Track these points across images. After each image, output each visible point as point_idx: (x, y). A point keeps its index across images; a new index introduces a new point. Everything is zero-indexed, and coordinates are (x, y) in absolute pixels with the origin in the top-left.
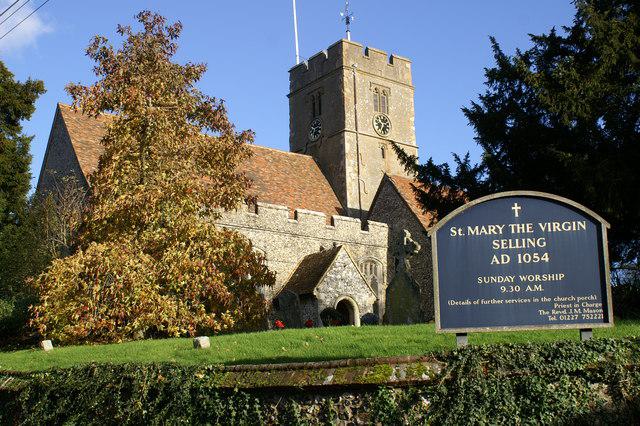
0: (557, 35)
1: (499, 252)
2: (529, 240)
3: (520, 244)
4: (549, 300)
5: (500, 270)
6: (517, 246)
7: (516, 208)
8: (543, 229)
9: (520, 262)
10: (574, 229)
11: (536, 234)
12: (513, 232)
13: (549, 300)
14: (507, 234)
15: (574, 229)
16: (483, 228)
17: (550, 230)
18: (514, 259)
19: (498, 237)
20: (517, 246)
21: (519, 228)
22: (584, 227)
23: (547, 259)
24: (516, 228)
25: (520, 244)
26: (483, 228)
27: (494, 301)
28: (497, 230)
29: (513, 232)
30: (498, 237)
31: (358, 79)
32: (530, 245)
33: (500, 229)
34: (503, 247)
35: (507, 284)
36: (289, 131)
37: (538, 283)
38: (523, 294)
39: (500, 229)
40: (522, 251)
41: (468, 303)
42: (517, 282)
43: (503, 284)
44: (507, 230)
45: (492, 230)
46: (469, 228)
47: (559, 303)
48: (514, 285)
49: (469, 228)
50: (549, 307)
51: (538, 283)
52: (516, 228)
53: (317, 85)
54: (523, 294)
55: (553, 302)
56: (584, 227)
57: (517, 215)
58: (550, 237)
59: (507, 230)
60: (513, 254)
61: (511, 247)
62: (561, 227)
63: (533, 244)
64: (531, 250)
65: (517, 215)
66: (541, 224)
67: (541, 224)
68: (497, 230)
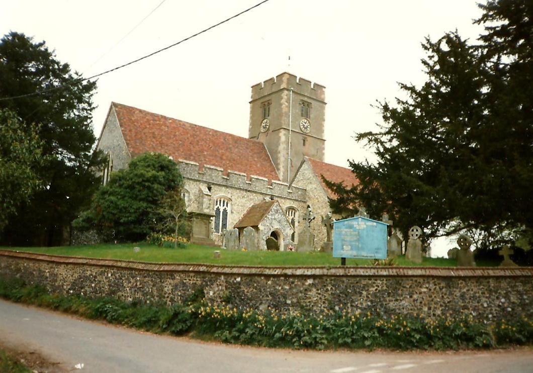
53: (267, 99)
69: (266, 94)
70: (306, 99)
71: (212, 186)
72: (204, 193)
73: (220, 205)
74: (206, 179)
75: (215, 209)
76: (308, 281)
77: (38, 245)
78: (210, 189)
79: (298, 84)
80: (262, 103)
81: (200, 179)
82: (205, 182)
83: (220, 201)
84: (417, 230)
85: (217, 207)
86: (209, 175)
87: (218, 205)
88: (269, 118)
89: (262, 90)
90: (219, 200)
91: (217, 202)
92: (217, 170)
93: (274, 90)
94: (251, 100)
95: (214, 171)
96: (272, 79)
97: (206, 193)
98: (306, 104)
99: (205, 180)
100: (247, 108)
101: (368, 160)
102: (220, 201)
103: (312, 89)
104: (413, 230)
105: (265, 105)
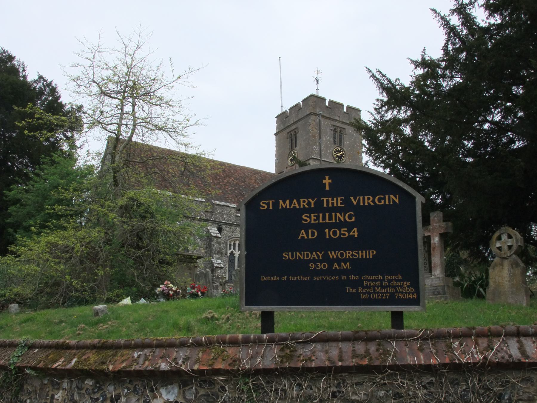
0: (427, 58)
1: (307, 227)
2: (338, 214)
3: (331, 218)
4: (357, 278)
5: (309, 245)
6: (327, 221)
7: (327, 181)
8: (355, 203)
9: (327, 237)
10: (387, 203)
11: (347, 207)
12: (325, 205)
13: (357, 278)
14: (319, 208)
15: (387, 203)
16: (295, 201)
17: (362, 204)
18: (322, 234)
19: (309, 211)
20: (327, 221)
21: (330, 202)
22: (397, 201)
23: (356, 234)
24: (328, 201)
25: (331, 218)
26: (295, 201)
27: (301, 278)
28: (309, 204)
29: (325, 205)
30: (309, 211)
31: (322, 123)
32: (339, 219)
33: (312, 202)
34: (313, 222)
35: (314, 261)
36: (275, 158)
37: (345, 261)
38: (330, 272)
39: (312, 202)
40: (330, 226)
41: (276, 278)
42: (326, 258)
43: (310, 261)
44: (319, 204)
45: (303, 203)
46: (281, 202)
47: (369, 281)
48: (321, 262)
49: (281, 202)
50: (356, 284)
51: (345, 261)
52: (328, 201)
53: (293, 127)
54: (330, 272)
55: (386, 282)
56: (397, 201)
57: (327, 188)
58: (359, 210)
59: (319, 204)
60: (321, 228)
61: (321, 221)
62: (373, 201)
63: (342, 219)
64: (340, 225)
65: (327, 188)
66: (352, 198)
67: (352, 198)
68: (309, 204)
69: (292, 122)
70: (339, 124)
71: (224, 227)
72: (213, 234)
73: (234, 249)
74: (216, 218)
75: (229, 254)
76: (163, 391)
77: (253, 305)
78: (220, 230)
79: (327, 107)
80: (288, 133)
81: (208, 218)
82: (215, 222)
83: (235, 244)
84: (510, 237)
85: (230, 251)
86: (219, 213)
87: (232, 250)
88: (297, 148)
89: (287, 119)
90: (232, 243)
91: (230, 245)
92: (229, 206)
93: (300, 116)
94: (275, 132)
95: (224, 209)
96: (297, 105)
97: (215, 235)
98: (339, 130)
99: (213, 219)
100: (272, 142)
101: (426, 51)
102: (235, 244)
103: (345, 113)
104: (499, 238)
105: (291, 134)
